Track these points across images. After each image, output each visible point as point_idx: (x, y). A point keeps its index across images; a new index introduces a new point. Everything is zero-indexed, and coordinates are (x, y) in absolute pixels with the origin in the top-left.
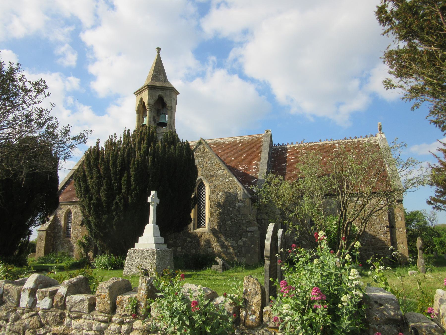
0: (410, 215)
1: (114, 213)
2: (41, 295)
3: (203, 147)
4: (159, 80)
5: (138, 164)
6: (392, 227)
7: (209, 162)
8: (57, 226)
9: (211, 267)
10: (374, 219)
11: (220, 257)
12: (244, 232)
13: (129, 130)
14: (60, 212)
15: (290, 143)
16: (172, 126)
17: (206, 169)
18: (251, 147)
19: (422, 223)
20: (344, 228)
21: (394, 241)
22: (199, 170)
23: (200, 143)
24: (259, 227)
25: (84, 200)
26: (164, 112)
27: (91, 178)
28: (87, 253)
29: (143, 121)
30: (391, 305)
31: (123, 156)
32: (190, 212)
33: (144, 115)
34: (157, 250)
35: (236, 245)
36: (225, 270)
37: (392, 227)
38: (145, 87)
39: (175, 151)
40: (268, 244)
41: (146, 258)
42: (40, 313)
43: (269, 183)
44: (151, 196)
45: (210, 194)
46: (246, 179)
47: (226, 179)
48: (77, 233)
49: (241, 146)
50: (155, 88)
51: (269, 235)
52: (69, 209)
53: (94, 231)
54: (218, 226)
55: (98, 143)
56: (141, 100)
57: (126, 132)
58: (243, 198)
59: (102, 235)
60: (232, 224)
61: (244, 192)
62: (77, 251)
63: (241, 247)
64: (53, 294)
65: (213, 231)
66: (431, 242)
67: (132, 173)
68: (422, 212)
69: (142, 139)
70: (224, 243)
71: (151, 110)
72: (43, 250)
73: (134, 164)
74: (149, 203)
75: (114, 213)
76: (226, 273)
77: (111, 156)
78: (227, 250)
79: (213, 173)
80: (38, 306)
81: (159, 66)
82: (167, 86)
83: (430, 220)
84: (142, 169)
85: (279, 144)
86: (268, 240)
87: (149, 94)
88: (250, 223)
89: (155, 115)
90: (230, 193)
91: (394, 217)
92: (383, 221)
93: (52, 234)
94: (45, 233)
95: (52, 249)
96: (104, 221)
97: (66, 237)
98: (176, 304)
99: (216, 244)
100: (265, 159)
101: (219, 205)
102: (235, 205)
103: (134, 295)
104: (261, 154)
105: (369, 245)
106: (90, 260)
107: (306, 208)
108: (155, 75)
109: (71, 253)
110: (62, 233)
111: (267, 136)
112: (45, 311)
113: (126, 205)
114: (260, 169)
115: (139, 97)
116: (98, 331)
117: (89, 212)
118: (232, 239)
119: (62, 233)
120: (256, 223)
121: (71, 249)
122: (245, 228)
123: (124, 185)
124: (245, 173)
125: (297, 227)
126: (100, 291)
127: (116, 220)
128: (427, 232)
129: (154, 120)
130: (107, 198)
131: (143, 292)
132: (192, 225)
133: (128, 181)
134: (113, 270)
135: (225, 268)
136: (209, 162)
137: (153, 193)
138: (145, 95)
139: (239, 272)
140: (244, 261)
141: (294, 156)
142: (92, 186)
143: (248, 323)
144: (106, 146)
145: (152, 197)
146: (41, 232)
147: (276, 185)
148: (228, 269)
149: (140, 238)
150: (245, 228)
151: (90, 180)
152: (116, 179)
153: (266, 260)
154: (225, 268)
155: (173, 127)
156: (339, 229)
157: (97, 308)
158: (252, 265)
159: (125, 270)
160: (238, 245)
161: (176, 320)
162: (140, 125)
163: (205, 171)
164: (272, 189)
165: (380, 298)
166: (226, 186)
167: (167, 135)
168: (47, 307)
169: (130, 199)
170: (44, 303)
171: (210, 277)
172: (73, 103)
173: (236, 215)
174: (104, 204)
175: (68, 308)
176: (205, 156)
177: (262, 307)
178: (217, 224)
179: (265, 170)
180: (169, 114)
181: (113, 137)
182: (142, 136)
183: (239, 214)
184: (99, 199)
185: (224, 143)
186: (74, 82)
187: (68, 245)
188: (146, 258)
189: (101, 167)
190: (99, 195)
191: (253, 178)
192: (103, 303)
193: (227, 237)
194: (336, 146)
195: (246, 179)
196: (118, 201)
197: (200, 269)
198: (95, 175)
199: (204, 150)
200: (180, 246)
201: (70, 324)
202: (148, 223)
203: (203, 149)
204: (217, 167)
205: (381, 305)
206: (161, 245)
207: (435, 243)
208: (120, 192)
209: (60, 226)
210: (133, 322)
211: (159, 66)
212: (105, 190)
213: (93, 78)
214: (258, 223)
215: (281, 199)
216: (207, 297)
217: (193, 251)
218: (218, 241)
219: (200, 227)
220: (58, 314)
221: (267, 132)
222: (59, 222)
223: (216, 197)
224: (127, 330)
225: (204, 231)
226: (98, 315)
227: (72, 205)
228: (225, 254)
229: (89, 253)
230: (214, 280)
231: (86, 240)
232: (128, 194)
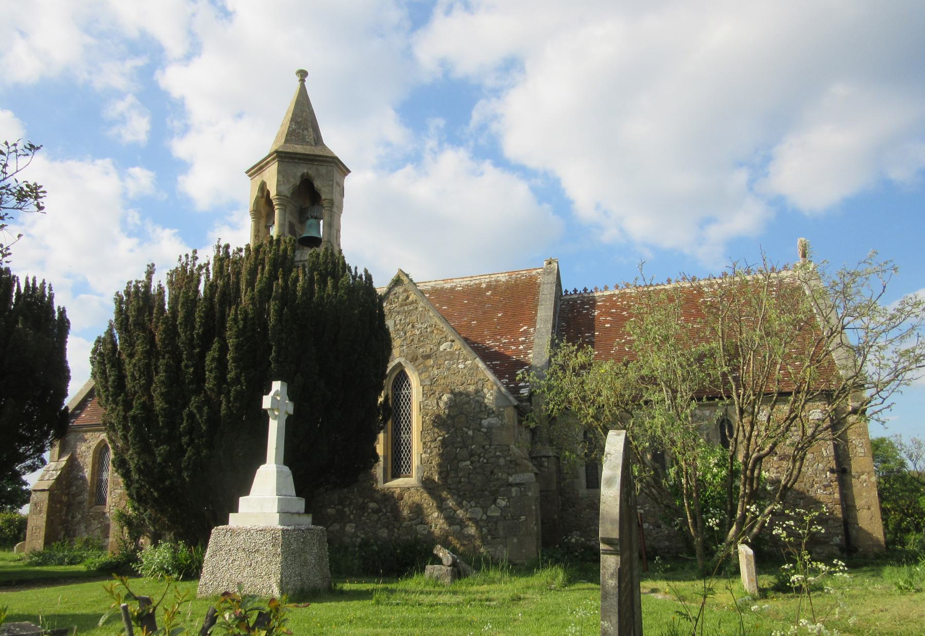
1: (185, 440)
3: (405, 291)
4: (303, 141)
5: (245, 319)
6: (842, 471)
7: (419, 326)
9: (423, 570)
11: (446, 545)
12: (502, 486)
13: (227, 247)
14: (83, 448)
15: (601, 287)
17: (412, 340)
18: (515, 296)
19: (892, 464)
20: (748, 472)
21: (849, 503)
22: (396, 343)
23: (397, 282)
24: (536, 474)
27: (131, 356)
32: (374, 439)
33: (270, 215)
34: (283, 531)
35: (484, 517)
36: (460, 578)
37: (842, 471)
38: (270, 155)
39: (337, 292)
41: (258, 551)
44: (272, 393)
45: (421, 398)
46: (505, 366)
47: (458, 364)
49: (492, 295)
50: (293, 158)
53: (137, 485)
54: (440, 474)
55: (150, 273)
56: (263, 187)
59: (156, 494)
60: (475, 468)
62: (116, 534)
63: (496, 523)
65: (427, 484)
67: (231, 342)
68: (893, 440)
70: (455, 511)
71: (284, 208)
72: (43, 533)
73: (235, 320)
74: (266, 411)
75: (185, 440)
76: (462, 585)
77: (181, 300)
78: (462, 529)
79: (428, 350)
82: (321, 153)
83: (910, 457)
84: (254, 328)
85: (575, 291)
87: (279, 172)
88: (517, 464)
89: (294, 221)
92: (823, 457)
93: (65, 499)
94: (46, 494)
95: (63, 533)
96: (159, 460)
100: (546, 321)
102: (480, 424)
107: (659, 420)
108: (294, 130)
110: (86, 496)
111: (550, 273)
113: (214, 420)
114: (537, 344)
115: (258, 180)
117: (125, 437)
118: (473, 503)
119: (86, 496)
120: (530, 464)
122: (505, 476)
123: (211, 371)
124: (502, 354)
127: (189, 458)
128: (905, 485)
129: (292, 231)
130: (167, 403)
132: (379, 470)
133: (221, 362)
134: (183, 580)
135: (458, 573)
136: (419, 326)
137: (277, 386)
139: (494, 582)
140: (504, 553)
141: (611, 314)
142: (133, 375)
144: (170, 283)
145: (275, 397)
146: (39, 493)
148: (466, 575)
149: (242, 500)
150: (505, 476)
151: (127, 361)
152: (191, 356)
153: (606, 552)
154: (458, 573)
158: (523, 564)
159: (202, 580)
160: (488, 517)
163: (409, 346)
164: (567, 381)
169: (223, 406)
171: (422, 596)
172: (139, 222)
173: (483, 447)
174: (161, 419)
182: (260, 257)
183: (490, 445)
184: (147, 408)
185: (452, 289)
186: (142, 178)
187: (100, 523)
188: (258, 551)
190: (151, 398)
193: (461, 498)
195: (505, 366)
196: (195, 411)
197: (398, 576)
198: (139, 349)
199: (408, 297)
200: (351, 522)
203: (405, 294)
204: (436, 337)
206: (296, 517)
208: (199, 390)
209: (83, 478)
213: (183, 167)
215: (593, 403)
217: (384, 533)
218: (441, 508)
219: (399, 477)
221: (550, 263)
222: (81, 469)
223: (435, 405)
225: (407, 484)
228: (458, 539)
229: (142, 540)
230: (432, 606)
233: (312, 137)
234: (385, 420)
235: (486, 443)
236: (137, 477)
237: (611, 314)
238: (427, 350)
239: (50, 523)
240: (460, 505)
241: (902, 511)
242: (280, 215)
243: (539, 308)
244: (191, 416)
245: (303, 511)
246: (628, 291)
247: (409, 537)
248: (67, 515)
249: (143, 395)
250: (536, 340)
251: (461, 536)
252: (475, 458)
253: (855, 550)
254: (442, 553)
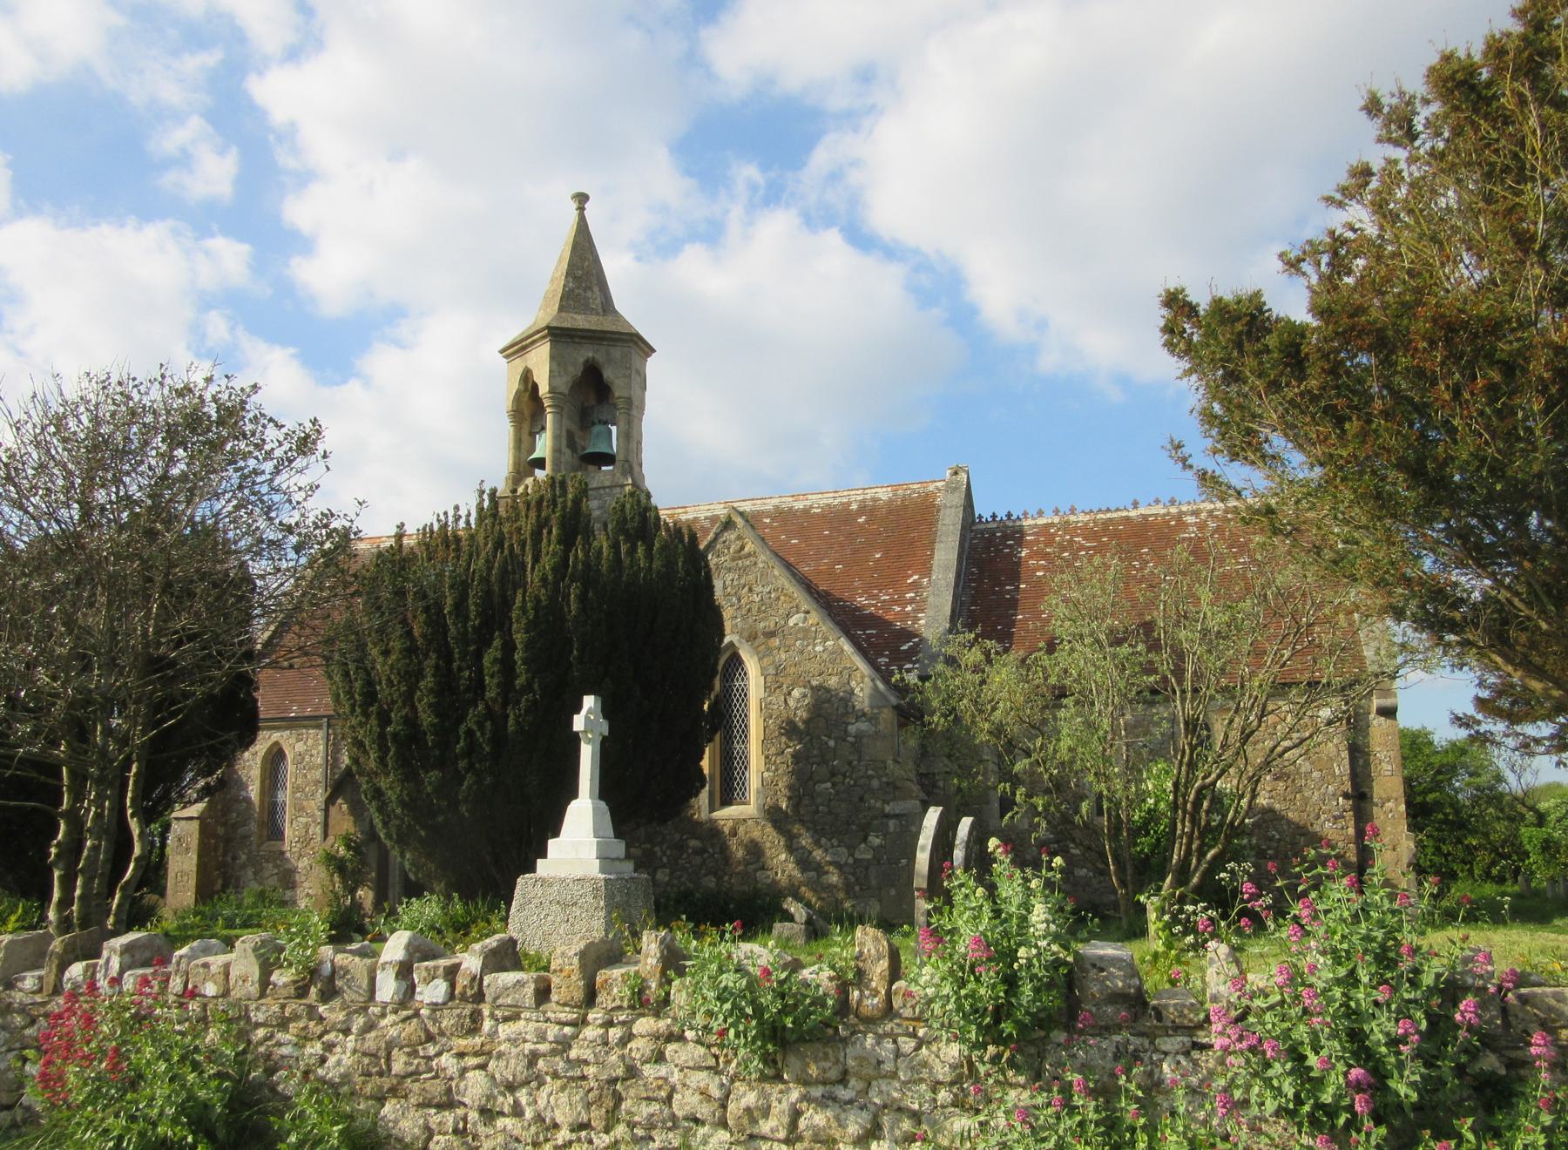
0: (1447, 752)
1: (462, 764)
2: (424, 974)
3: (739, 538)
4: (585, 308)
5: (536, 609)
6: (1360, 797)
7: (760, 589)
8: (237, 800)
10: (1303, 770)
11: (798, 898)
12: (875, 818)
13: (493, 492)
15: (1032, 511)
16: (631, 468)
18: (903, 525)
22: (727, 614)
25: (361, 725)
26: (604, 418)
27: (386, 653)
28: (353, 891)
29: (533, 450)
30: (1120, 969)
31: (488, 581)
35: (851, 861)
37: (1360, 797)
38: (538, 332)
40: (923, 858)
41: (575, 904)
42: (424, 1012)
43: (951, 661)
45: (762, 694)
46: (882, 641)
48: (307, 826)
49: (867, 522)
50: (572, 337)
51: (926, 838)
52: (276, 743)
54: (789, 798)
56: (527, 376)
57: (485, 497)
58: (872, 707)
60: (837, 793)
61: (876, 688)
63: (867, 869)
64: (452, 973)
65: (774, 816)
66: (1513, 844)
67: (519, 638)
69: (542, 524)
72: (192, 882)
73: (523, 609)
75: (462, 764)
78: (819, 877)
80: (418, 997)
81: (583, 259)
82: (613, 328)
84: (548, 619)
85: (994, 516)
86: (923, 848)
87: (552, 358)
88: (896, 788)
89: (574, 428)
90: (828, 690)
91: (1367, 764)
93: (221, 831)
94: (195, 825)
95: (220, 882)
96: (429, 789)
97: (269, 839)
98: (728, 979)
99: (783, 856)
100: (947, 568)
101: (790, 729)
102: (846, 731)
103: (633, 969)
104: (933, 550)
106: (365, 916)
108: (572, 290)
109: (289, 893)
110: (253, 826)
111: (956, 489)
112: (435, 1007)
113: (499, 739)
114: (931, 606)
115: (519, 365)
116: (557, 1042)
117: (382, 760)
119: (253, 826)
120: (915, 788)
121: (288, 879)
122: (878, 805)
123: (492, 676)
125: (1039, 802)
126: (559, 961)
127: (469, 788)
128: (1502, 810)
129: (572, 444)
130: (436, 716)
131: (652, 961)
132: (704, 795)
137: (589, 701)
138: (540, 361)
141: (1045, 556)
143: (864, 1011)
145: (587, 716)
147: (976, 669)
149: (551, 843)
151: (380, 660)
155: (636, 469)
156: (1175, 806)
157: (554, 997)
161: (727, 1006)
162: (526, 465)
165: (1101, 958)
166: (813, 667)
167: (623, 506)
168: (440, 1000)
169: (511, 721)
170: (432, 992)
173: (850, 763)
174: (430, 738)
175: (488, 998)
176: (745, 568)
177: (891, 983)
178: (786, 792)
179: (948, 610)
180: (622, 424)
181: (451, 519)
183: (860, 760)
184: (411, 722)
186: (230, 258)
187: (276, 866)
189: (415, 617)
190: (414, 708)
191: (907, 635)
192: (567, 985)
193: (819, 833)
194: (1187, 525)
195: (882, 641)
198: (396, 645)
199: (742, 548)
200: (664, 866)
201: (496, 1032)
202: (576, 796)
203: (739, 543)
205: (1102, 970)
207: (1528, 847)
209: (248, 800)
210: (633, 1021)
211: (583, 259)
212: (431, 691)
214: (922, 785)
216: (784, 967)
217: (710, 882)
218: (790, 849)
220: (467, 1012)
222: (244, 786)
223: (782, 703)
224: (621, 1039)
225: (743, 815)
226: (553, 1010)
227: (287, 728)
228: (815, 891)
229: (360, 892)
231: (348, 847)
232: (505, 705)
233: (598, 301)
234: (714, 731)
235: (854, 757)
236: (398, 811)
237: (1045, 556)
238: (770, 624)
239: (202, 867)
240: (817, 843)
241: (1495, 850)
242: (554, 422)
243: (937, 546)
244: (470, 733)
245: (622, 855)
246: (1072, 518)
247: (746, 888)
248: (225, 854)
249: (404, 706)
250: (931, 599)
251: (817, 886)
252: (839, 778)
254: (793, 907)
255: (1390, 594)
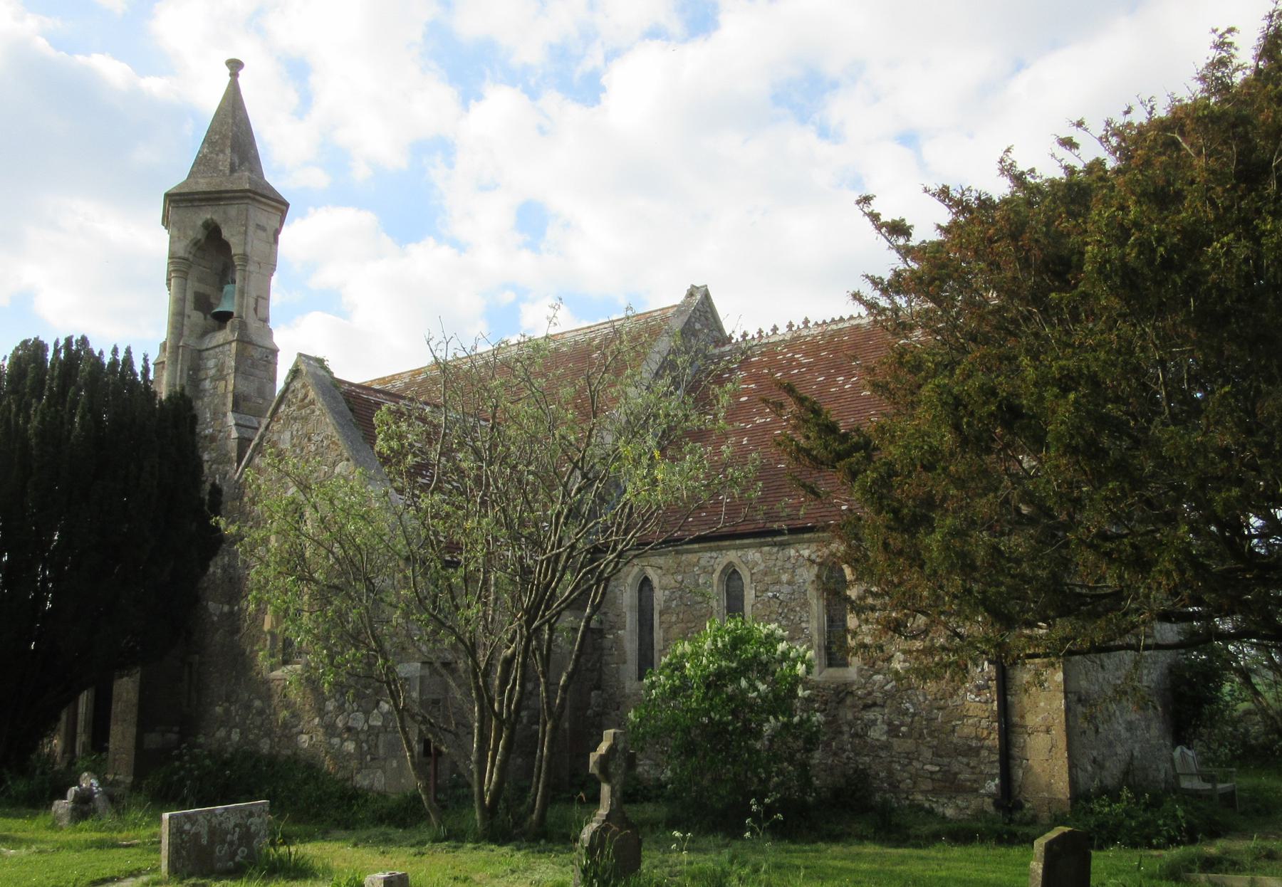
3: (304, 386)
35: (366, 728)
52: (730, 564)
63: (377, 736)
85: (745, 335)
105: (921, 735)
108: (205, 156)
199: (306, 396)
253: (1020, 806)
255: (806, 859)
